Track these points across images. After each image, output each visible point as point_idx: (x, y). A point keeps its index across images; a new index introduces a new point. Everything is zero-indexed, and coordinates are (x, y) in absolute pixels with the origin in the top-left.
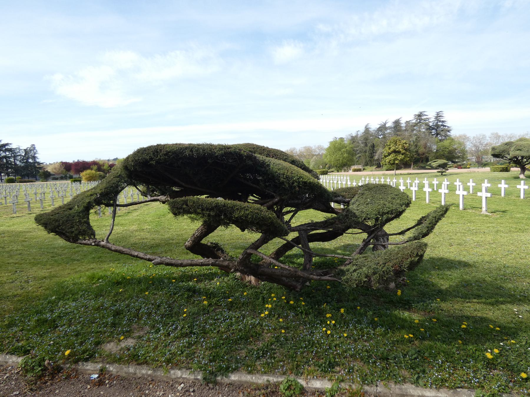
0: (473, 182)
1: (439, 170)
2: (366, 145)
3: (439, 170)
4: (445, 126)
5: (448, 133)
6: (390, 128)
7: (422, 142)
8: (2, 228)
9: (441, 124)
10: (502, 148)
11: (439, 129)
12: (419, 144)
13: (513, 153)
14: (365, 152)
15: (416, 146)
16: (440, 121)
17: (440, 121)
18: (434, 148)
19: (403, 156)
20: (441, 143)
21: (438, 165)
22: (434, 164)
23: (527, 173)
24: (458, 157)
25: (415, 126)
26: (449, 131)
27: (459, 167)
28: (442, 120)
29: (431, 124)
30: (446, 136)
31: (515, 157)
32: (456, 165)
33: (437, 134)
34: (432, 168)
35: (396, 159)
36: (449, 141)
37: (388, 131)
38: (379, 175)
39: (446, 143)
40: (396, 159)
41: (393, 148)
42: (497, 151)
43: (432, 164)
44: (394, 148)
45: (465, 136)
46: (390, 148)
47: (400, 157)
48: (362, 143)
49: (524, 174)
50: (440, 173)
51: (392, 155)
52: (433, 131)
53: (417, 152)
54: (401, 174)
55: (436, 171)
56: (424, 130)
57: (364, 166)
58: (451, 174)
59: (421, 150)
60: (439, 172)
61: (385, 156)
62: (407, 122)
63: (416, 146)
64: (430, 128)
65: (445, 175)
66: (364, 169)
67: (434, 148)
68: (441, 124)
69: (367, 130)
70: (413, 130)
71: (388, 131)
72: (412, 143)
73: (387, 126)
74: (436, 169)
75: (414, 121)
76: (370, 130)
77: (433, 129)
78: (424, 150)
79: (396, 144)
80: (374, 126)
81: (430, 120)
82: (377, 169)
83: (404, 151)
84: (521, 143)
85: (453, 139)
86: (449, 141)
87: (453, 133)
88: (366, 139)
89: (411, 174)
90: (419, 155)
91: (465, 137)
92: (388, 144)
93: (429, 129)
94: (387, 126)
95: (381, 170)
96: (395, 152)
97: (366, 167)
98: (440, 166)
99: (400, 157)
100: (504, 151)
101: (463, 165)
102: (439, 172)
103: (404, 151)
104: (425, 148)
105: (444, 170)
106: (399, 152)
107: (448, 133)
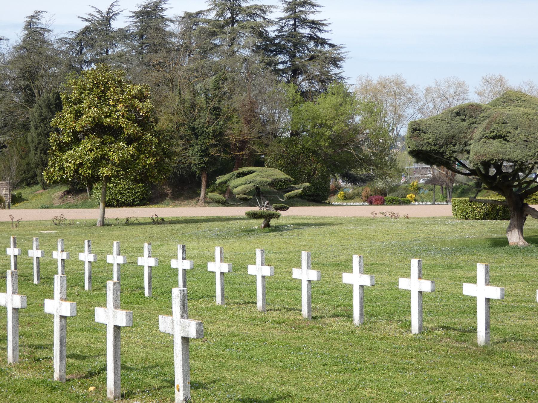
0: (266, 262)
1: (256, 209)
2: (30, 101)
3: (256, 209)
4: (323, 42)
5: (334, 70)
6: (124, 35)
7: (239, 100)
8: (534, 262)
9: (306, 31)
10: (444, 129)
11: (301, 52)
12: (224, 105)
13: (479, 149)
14: (26, 127)
15: (217, 112)
16: (304, 22)
17: (304, 22)
18: (284, 122)
19: (131, 149)
20: (306, 107)
21: (251, 186)
22: (239, 185)
23: (530, 223)
24: (367, 161)
25: (213, 34)
26: (335, 62)
27: (379, 198)
28: (311, 17)
29: (272, 31)
30: (325, 80)
31: (486, 164)
32: (367, 189)
33: (296, 72)
34: (231, 200)
35: (103, 159)
36: (333, 100)
37: (120, 48)
38: (38, 224)
39: (324, 106)
40: (103, 159)
41: (90, 115)
42: (429, 137)
43: (232, 183)
44: (92, 113)
45: (399, 84)
46: (78, 115)
47: (119, 152)
48: (16, 90)
49: (520, 228)
50: (262, 221)
51: (86, 144)
52: (281, 57)
53: (219, 135)
54: (128, 223)
55: (242, 211)
56: (247, 52)
57: (14, 187)
58: (299, 225)
59: (236, 130)
60: (254, 216)
61: (63, 148)
62: (189, 16)
63: (217, 112)
64: (268, 47)
65: (278, 229)
66: (16, 200)
67: (284, 122)
68: (306, 31)
69: (34, 34)
70: (205, 52)
71: (120, 48)
72: (201, 100)
73: (117, 24)
74: (245, 202)
75: (212, 16)
76: (51, 37)
77: (280, 49)
78: (245, 129)
79: (103, 97)
80: (64, 22)
81: (270, 16)
82: (70, 199)
83: (132, 129)
84: (506, 111)
85: (347, 95)
86: (333, 100)
87: (353, 74)
88: (30, 75)
89: (162, 222)
90: (226, 146)
91: (399, 91)
92: (75, 95)
93: (266, 49)
94: (117, 24)
95: (195, 205)
96: (98, 128)
97: (25, 192)
98: (257, 194)
99: (119, 152)
100: (450, 140)
101: (392, 189)
102: (254, 216)
103: (132, 129)
104: (248, 122)
105: (272, 210)
106: (115, 132)
107: (334, 70)
